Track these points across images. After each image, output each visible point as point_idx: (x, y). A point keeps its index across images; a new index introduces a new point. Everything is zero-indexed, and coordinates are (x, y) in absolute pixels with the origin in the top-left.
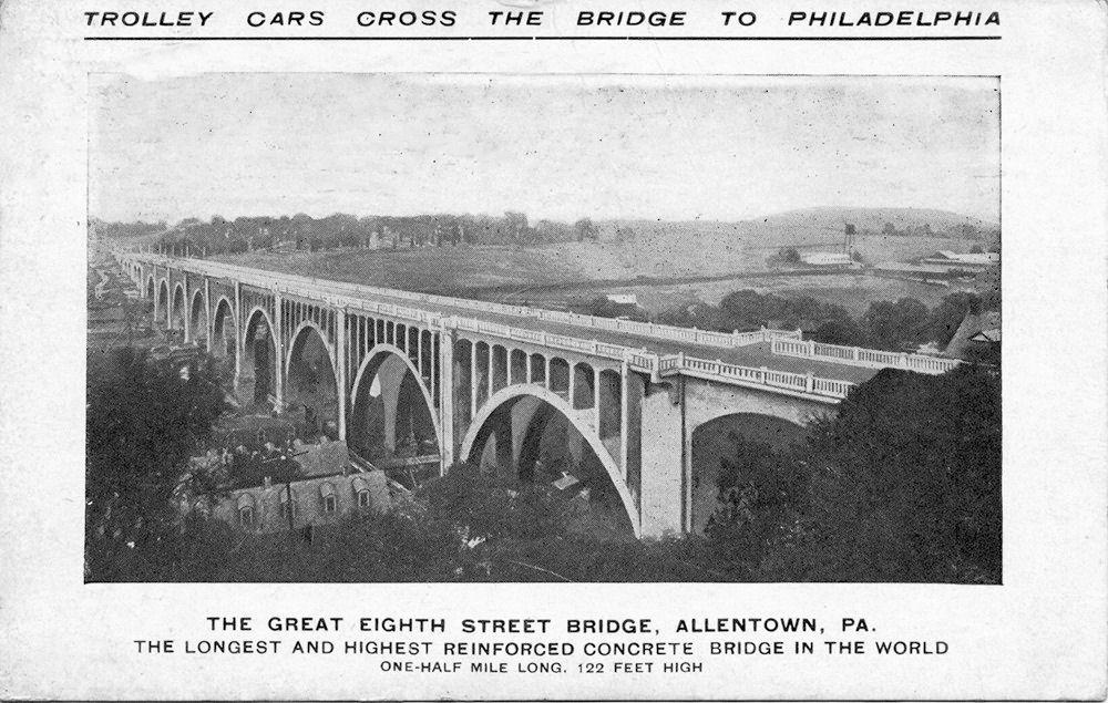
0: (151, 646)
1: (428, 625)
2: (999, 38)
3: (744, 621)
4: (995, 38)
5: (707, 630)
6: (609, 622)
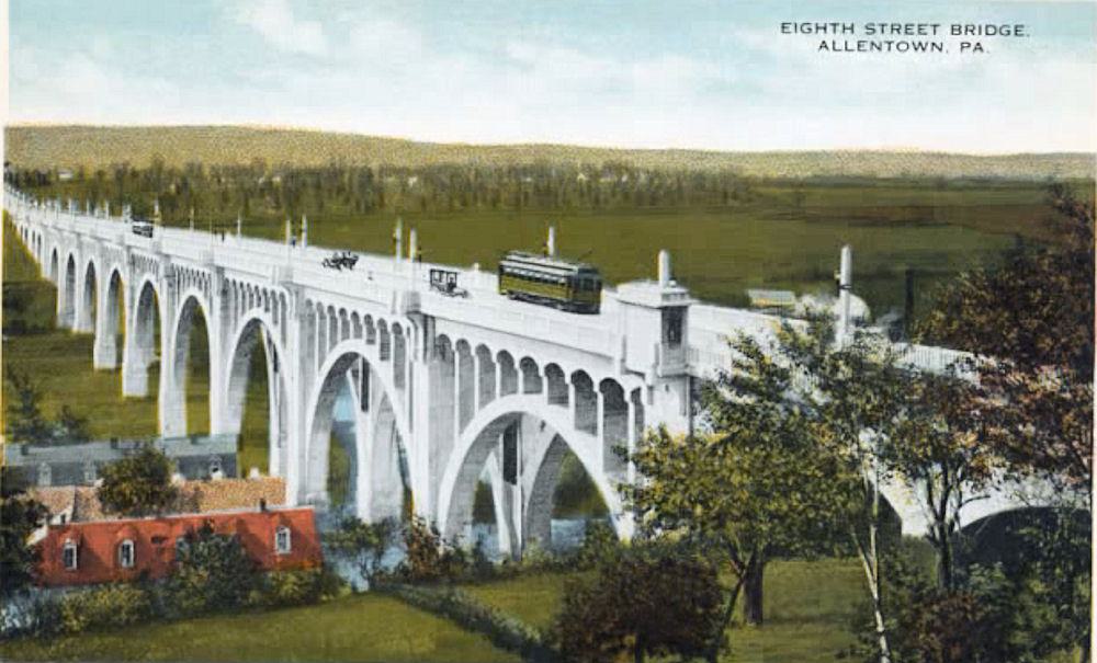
1: (840, 28)
6: (987, 27)
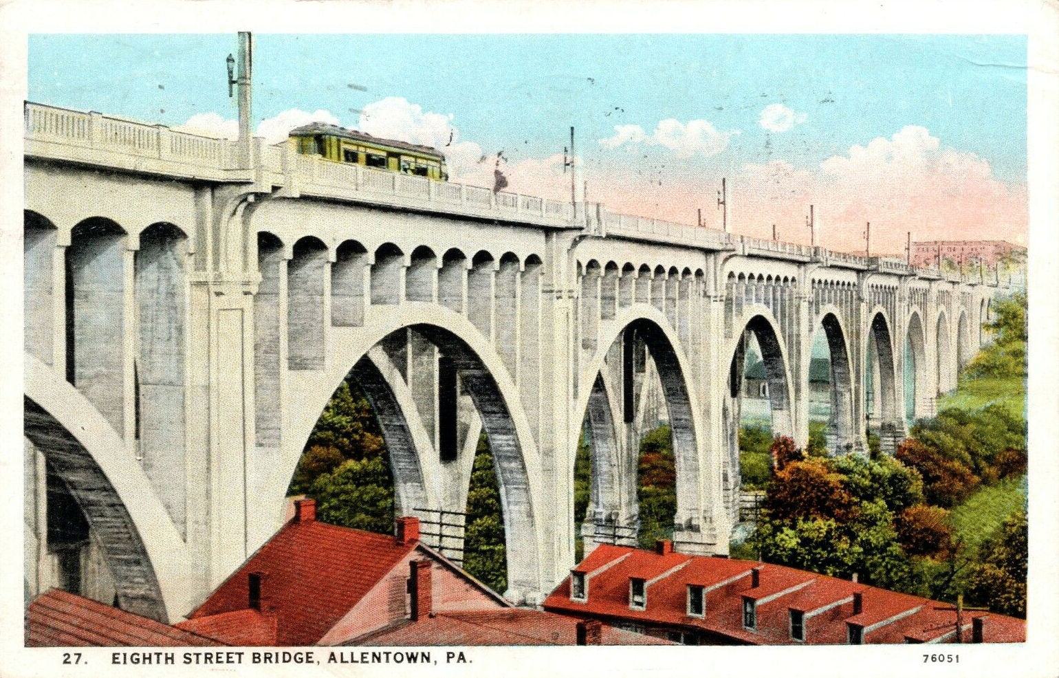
3: (380, 654)
5: (353, 661)
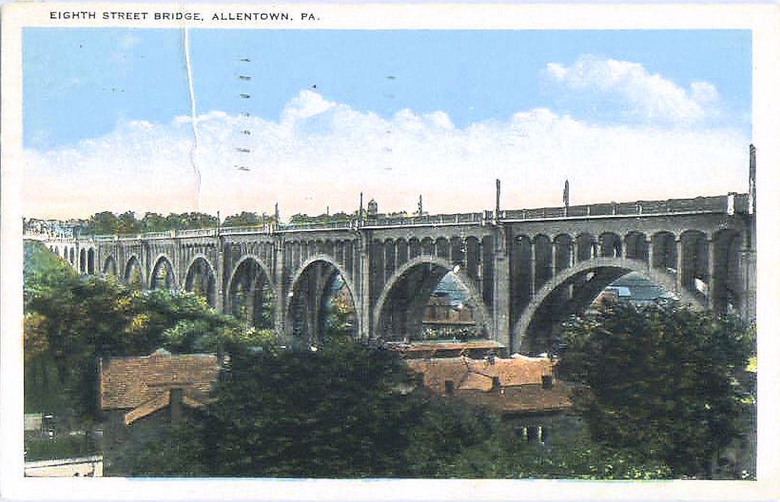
0: (90, 15)
2: (498, 182)
4: (498, 187)
5: (230, 19)
